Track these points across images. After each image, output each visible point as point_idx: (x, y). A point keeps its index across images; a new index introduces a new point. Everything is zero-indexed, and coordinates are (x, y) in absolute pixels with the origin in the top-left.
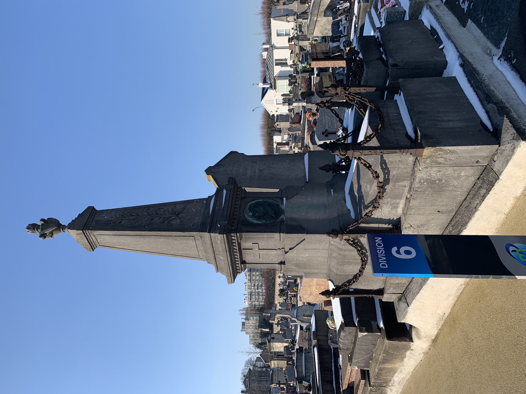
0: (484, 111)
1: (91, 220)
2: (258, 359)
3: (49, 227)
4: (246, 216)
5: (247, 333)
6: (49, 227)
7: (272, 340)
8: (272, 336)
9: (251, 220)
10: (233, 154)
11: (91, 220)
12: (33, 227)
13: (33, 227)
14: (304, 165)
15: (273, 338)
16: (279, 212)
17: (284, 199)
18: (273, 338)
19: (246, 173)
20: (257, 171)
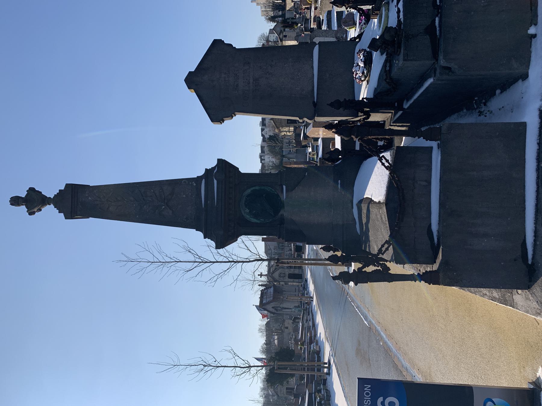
0: (536, 189)
1: (78, 201)
2: (271, 31)
3: (33, 201)
4: (243, 212)
5: (258, 4)
6: (33, 201)
7: (284, 38)
8: (284, 34)
9: (248, 217)
10: (215, 40)
11: (78, 201)
12: (16, 201)
13: (16, 201)
14: (313, 68)
15: (285, 36)
16: (276, 204)
17: (284, 187)
18: (285, 36)
19: (237, 86)
20: (251, 81)
